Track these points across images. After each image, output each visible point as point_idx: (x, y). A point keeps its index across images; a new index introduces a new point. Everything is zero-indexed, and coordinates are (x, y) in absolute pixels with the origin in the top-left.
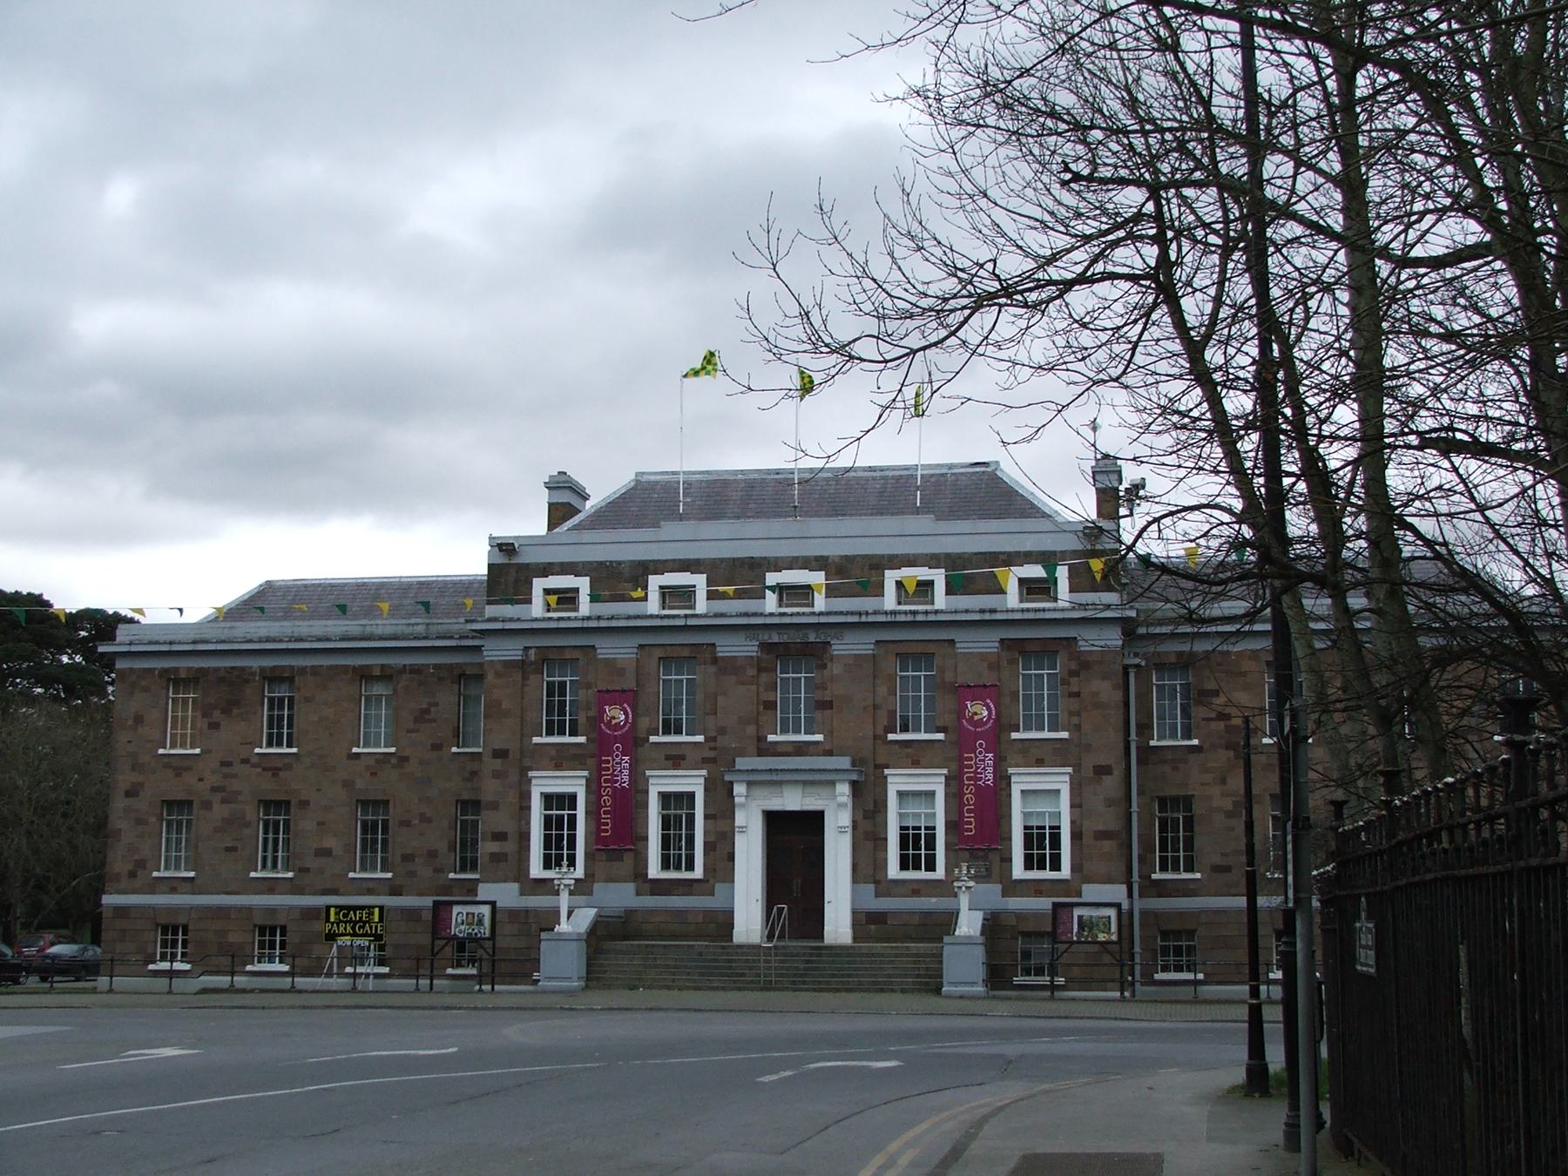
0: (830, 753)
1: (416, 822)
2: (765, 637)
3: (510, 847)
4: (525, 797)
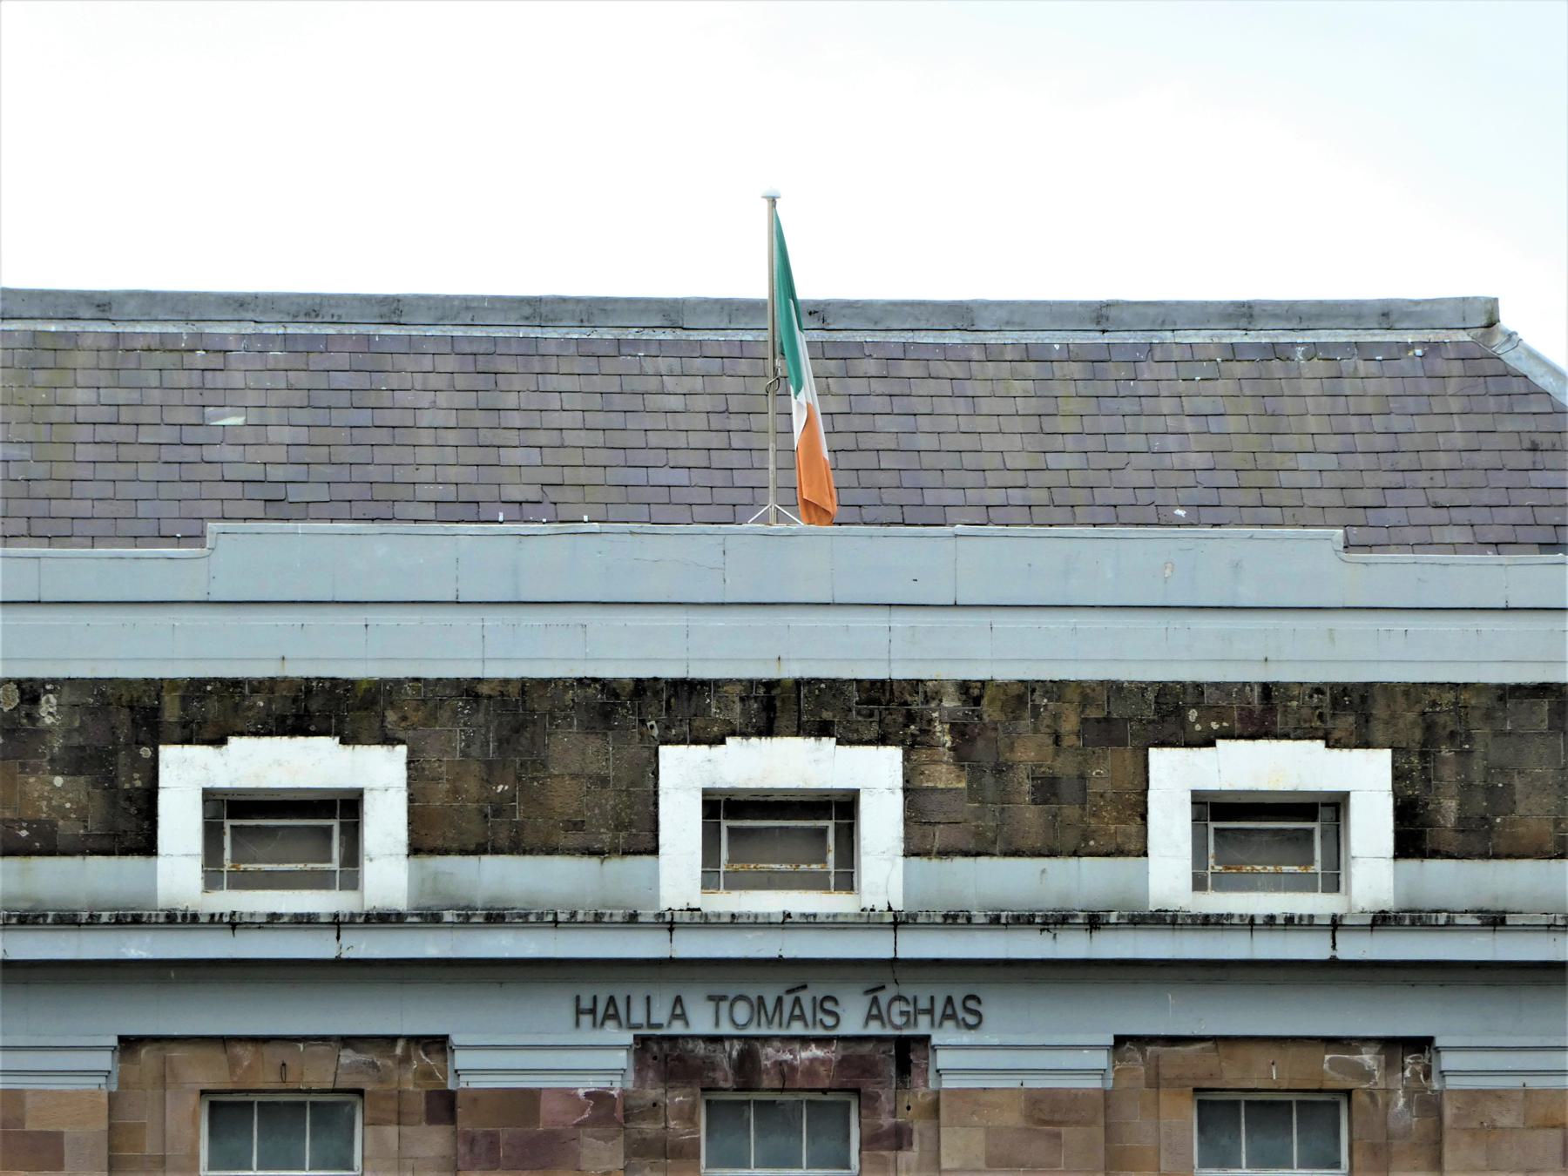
2: (656, 1010)
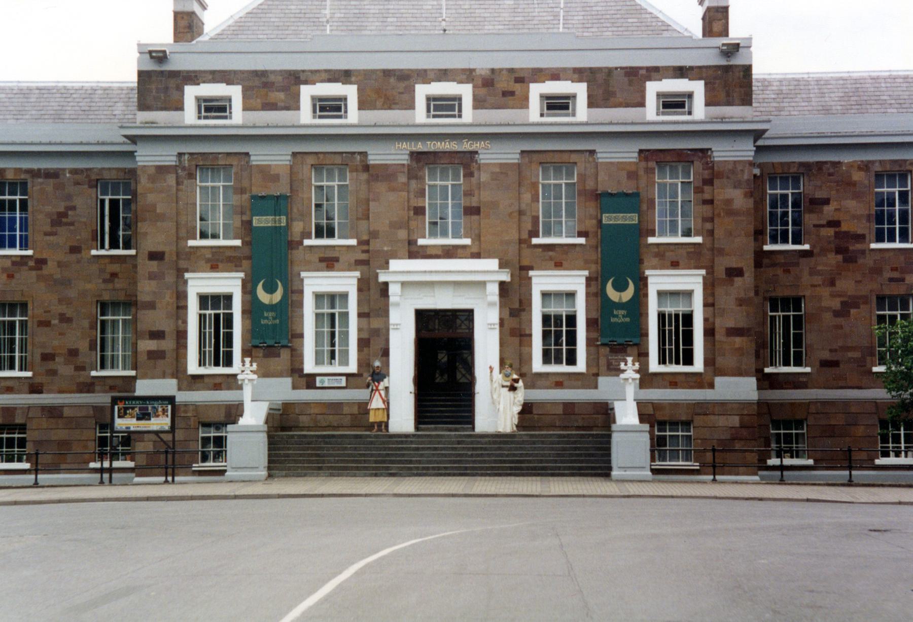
0: (477, 256)
1: (55, 322)
3: (167, 344)
4: (181, 297)
